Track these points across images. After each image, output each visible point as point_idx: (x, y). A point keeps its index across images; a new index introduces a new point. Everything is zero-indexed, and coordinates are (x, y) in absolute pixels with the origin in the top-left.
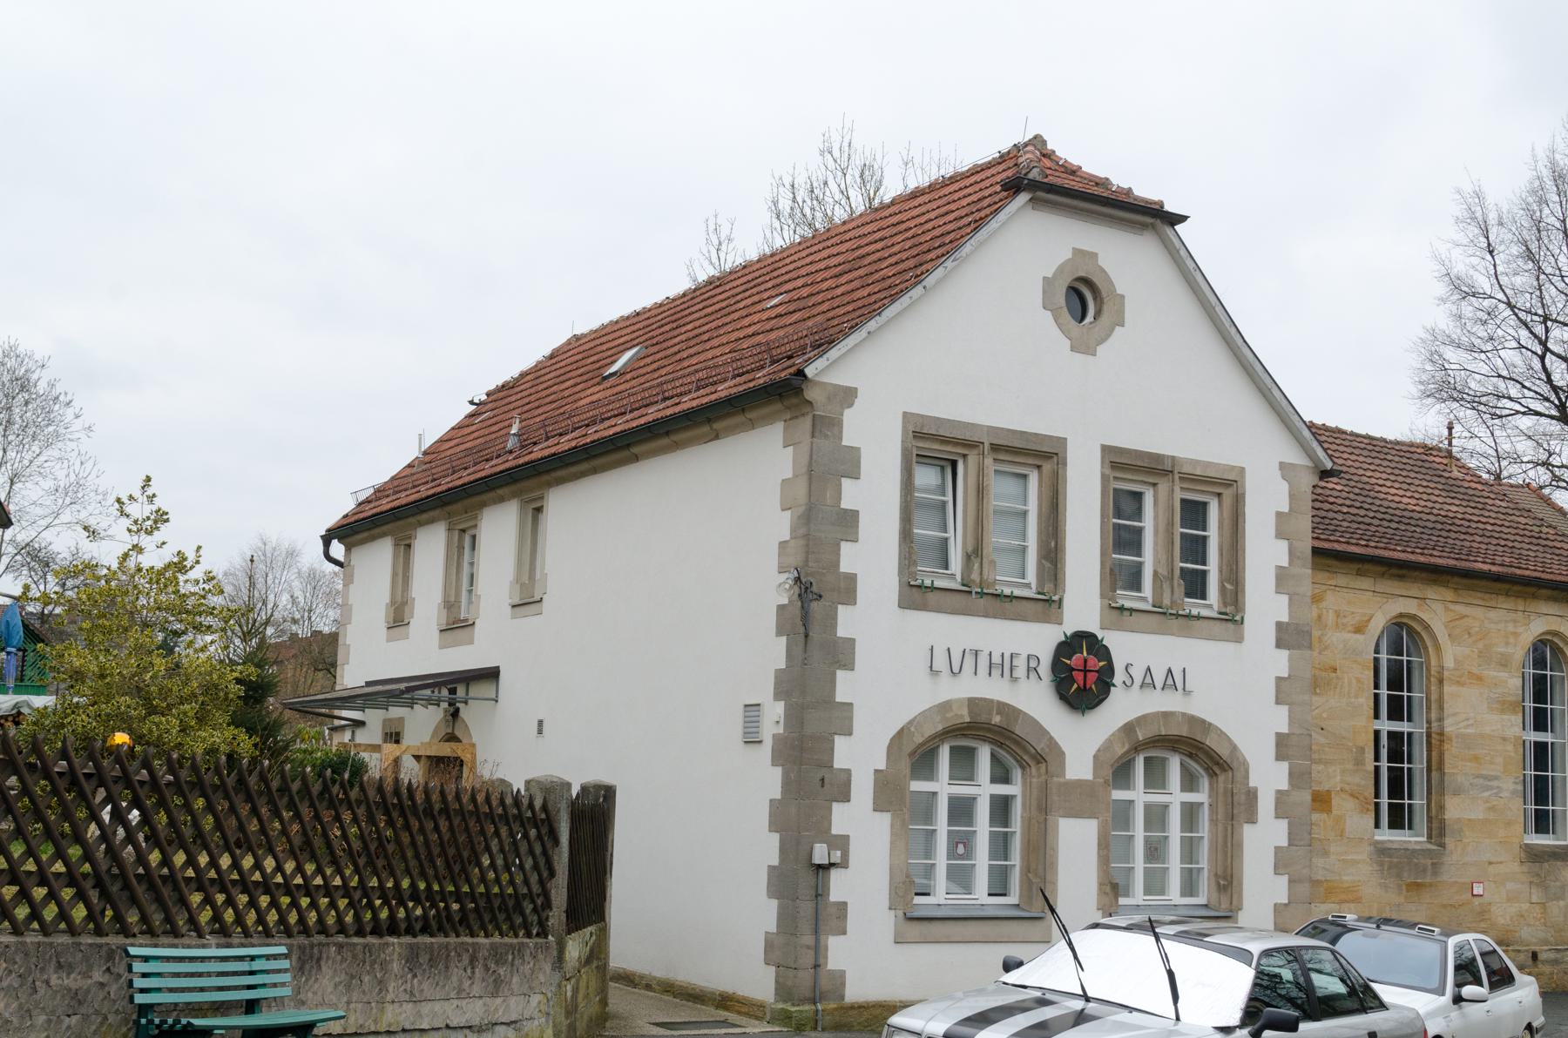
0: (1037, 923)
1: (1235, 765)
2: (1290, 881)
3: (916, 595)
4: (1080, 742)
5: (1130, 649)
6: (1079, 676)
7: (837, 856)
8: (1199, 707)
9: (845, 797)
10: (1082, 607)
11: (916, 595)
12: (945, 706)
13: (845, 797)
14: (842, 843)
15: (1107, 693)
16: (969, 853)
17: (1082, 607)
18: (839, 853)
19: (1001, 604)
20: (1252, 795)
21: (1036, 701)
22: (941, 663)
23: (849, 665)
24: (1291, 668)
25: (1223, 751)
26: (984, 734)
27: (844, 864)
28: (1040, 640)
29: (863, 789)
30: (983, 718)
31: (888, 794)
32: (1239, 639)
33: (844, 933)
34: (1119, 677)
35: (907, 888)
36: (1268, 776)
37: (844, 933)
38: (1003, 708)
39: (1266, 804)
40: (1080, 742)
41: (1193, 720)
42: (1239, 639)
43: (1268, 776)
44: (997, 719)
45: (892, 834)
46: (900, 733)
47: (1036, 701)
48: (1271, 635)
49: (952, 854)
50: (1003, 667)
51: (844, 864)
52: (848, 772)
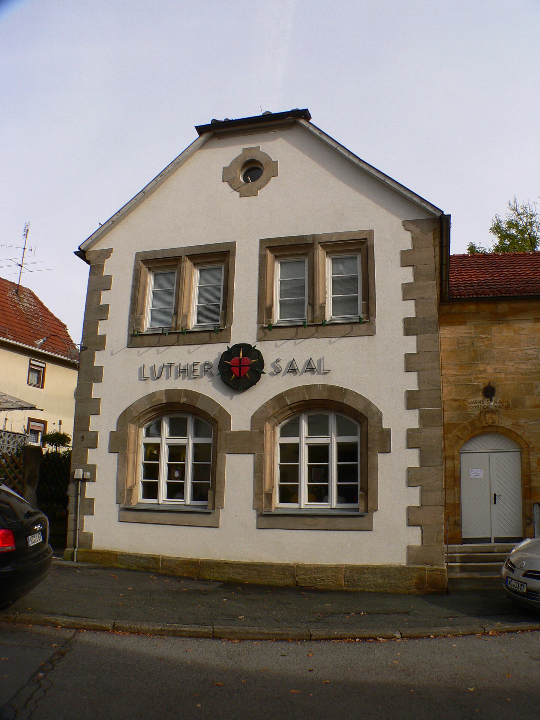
0: (209, 516)
1: (369, 415)
2: (422, 491)
3: (136, 338)
4: (241, 410)
5: (272, 352)
6: (236, 370)
7: (88, 475)
8: (336, 379)
9: (95, 446)
10: (243, 329)
11: (136, 338)
12: (153, 395)
13: (95, 446)
14: (92, 469)
15: (258, 378)
16: (182, 476)
17: (243, 329)
18: (88, 474)
19: (179, 335)
20: (386, 434)
21: (208, 388)
22: (147, 373)
23: (99, 380)
24: (418, 348)
25: (359, 407)
26: (176, 410)
27: (92, 479)
28: (212, 353)
29: (103, 441)
30: (175, 400)
31: (119, 443)
32: (372, 333)
33: (93, 515)
34: (268, 368)
35: (123, 494)
36: (399, 420)
37: (93, 515)
38: (188, 393)
39: (398, 440)
40: (241, 410)
41: (332, 389)
42: (372, 333)
43: (399, 420)
44: (184, 400)
45: (118, 464)
46: (125, 412)
47: (208, 388)
48: (400, 327)
49: (170, 476)
50: (185, 372)
51: (92, 479)
52: (97, 433)
